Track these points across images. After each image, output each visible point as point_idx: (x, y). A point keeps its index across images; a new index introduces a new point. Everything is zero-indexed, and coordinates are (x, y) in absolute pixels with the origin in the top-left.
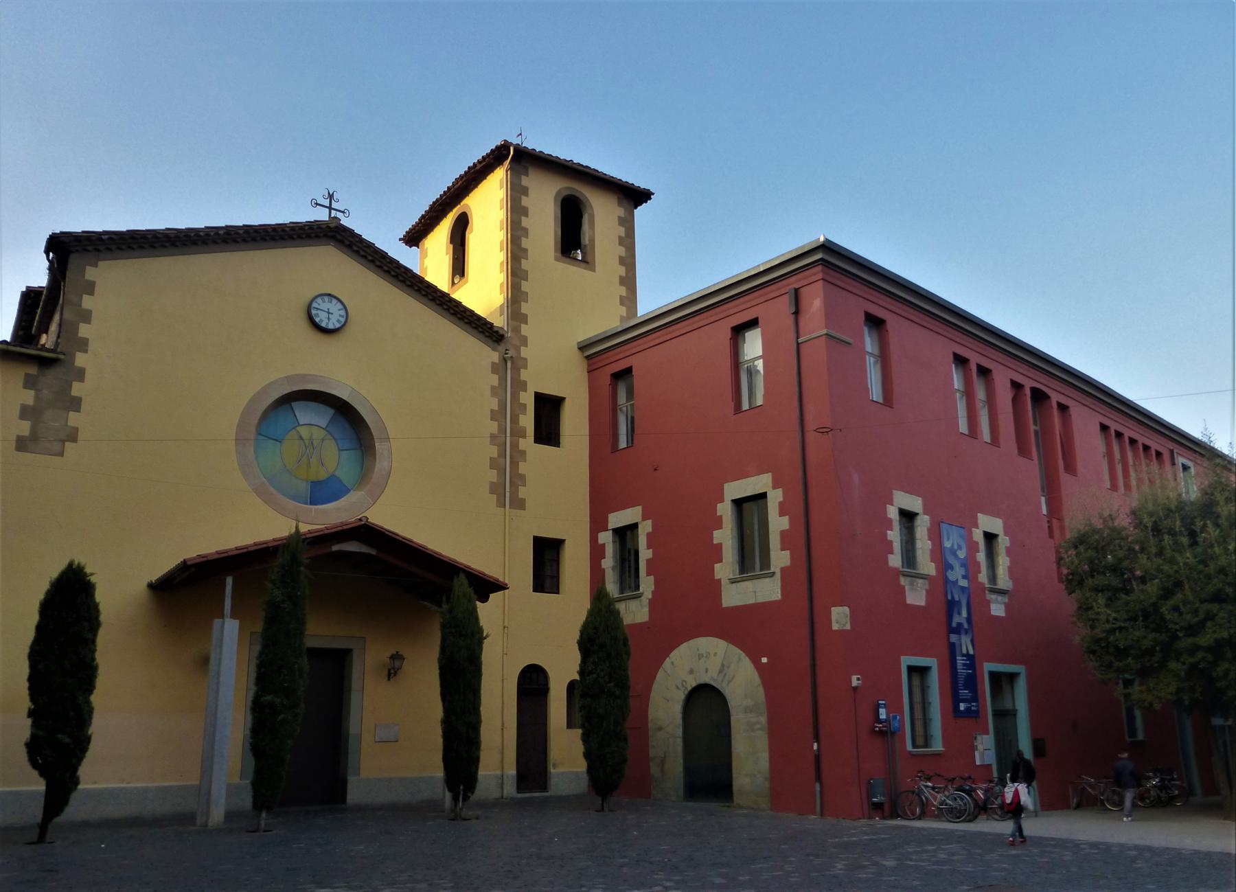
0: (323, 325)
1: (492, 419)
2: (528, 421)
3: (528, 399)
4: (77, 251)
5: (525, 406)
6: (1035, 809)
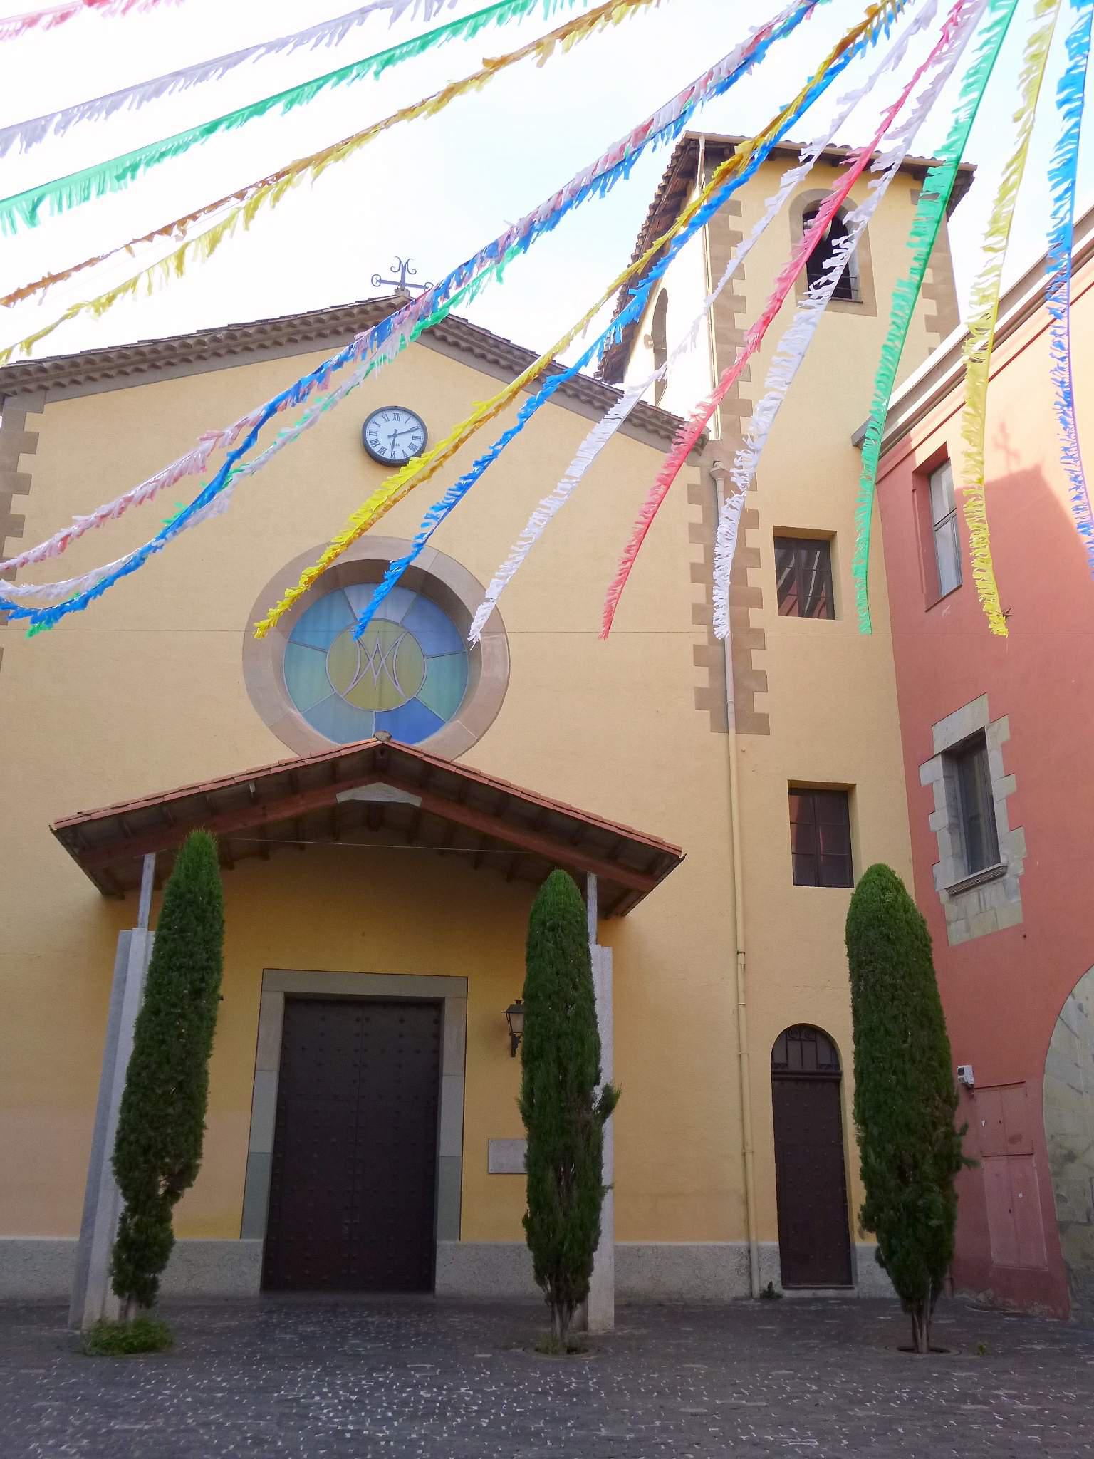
0: (387, 455)
1: (694, 580)
2: (765, 578)
3: (764, 542)
4: (15, 393)
5: (756, 552)
6: (693, 226)
